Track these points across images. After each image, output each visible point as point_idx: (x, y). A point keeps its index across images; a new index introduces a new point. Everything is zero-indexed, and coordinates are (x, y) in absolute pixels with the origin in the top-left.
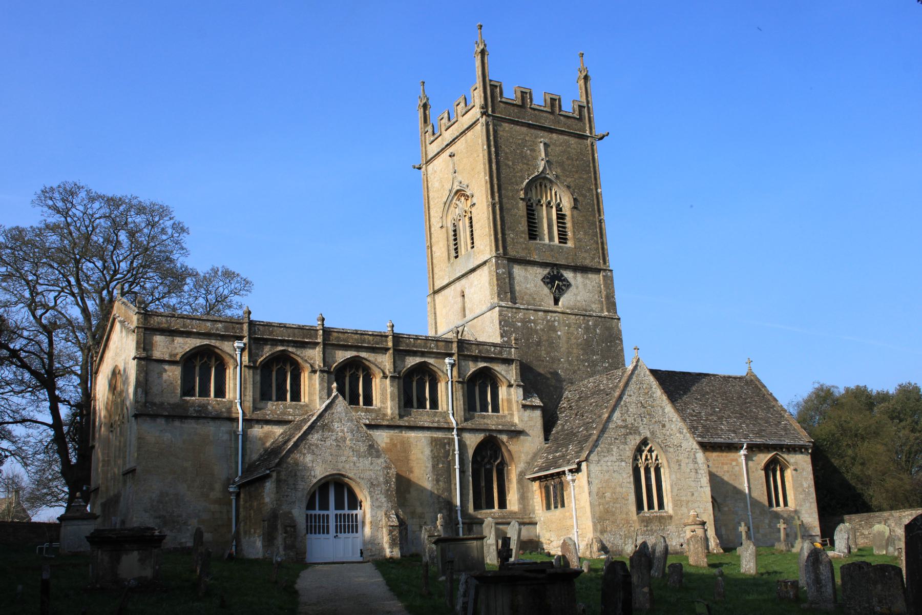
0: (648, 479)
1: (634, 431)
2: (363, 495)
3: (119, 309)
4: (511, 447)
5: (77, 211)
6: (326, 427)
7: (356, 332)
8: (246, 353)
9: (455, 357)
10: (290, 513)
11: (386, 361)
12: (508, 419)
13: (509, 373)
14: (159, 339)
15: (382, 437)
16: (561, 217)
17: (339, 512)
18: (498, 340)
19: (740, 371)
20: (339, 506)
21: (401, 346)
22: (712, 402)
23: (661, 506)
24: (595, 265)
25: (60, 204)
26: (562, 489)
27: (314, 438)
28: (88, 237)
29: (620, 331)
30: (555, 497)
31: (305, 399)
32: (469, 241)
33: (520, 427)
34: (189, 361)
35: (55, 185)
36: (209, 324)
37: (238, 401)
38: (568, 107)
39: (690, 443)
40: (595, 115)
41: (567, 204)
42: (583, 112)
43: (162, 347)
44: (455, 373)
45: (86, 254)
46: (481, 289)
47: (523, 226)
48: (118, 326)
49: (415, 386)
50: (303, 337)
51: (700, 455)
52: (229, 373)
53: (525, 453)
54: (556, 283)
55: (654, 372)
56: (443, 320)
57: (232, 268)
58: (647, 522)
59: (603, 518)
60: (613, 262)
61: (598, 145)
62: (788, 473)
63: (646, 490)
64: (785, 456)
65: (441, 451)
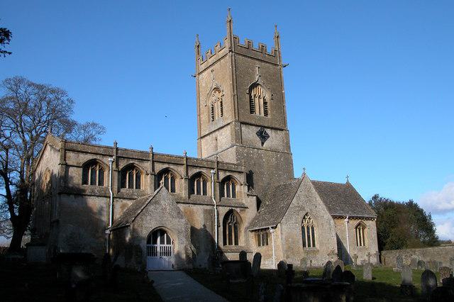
0: (308, 232)
1: (303, 209)
2: (173, 237)
3: (205, 131)
4: (242, 215)
5: (22, 91)
6: (157, 203)
7: (168, 156)
8: (114, 164)
9: (216, 170)
10: (139, 245)
11: (182, 170)
12: (240, 201)
13: (241, 179)
14: (70, 154)
15: (181, 207)
16: (265, 103)
17: (162, 245)
18: (235, 163)
19: (341, 180)
20: (162, 242)
21: (189, 163)
22: (340, 199)
23: (314, 245)
24: (281, 128)
25: (14, 87)
26: (267, 236)
27: (151, 208)
28: (26, 105)
29: (292, 160)
30: (263, 240)
31: (142, 188)
32: (220, 113)
33: (246, 205)
34: (87, 166)
35: (12, 78)
36: (96, 148)
37: (110, 188)
38: (269, 51)
39: (327, 216)
40: (282, 55)
41: (268, 97)
42: (276, 53)
43: (72, 158)
44: (216, 178)
45: (26, 112)
46: (225, 137)
47: (248, 107)
48: (48, 148)
49: (195, 181)
50: (142, 157)
51: (332, 221)
52: (106, 173)
53: (249, 215)
54: (263, 136)
55: (314, 183)
56: (206, 151)
57: (96, 122)
58: (307, 253)
59: (289, 249)
60: (289, 126)
61: (283, 69)
62: (366, 230)
63: (308, 237)
64: (365, 222)
65: (209, 214)
